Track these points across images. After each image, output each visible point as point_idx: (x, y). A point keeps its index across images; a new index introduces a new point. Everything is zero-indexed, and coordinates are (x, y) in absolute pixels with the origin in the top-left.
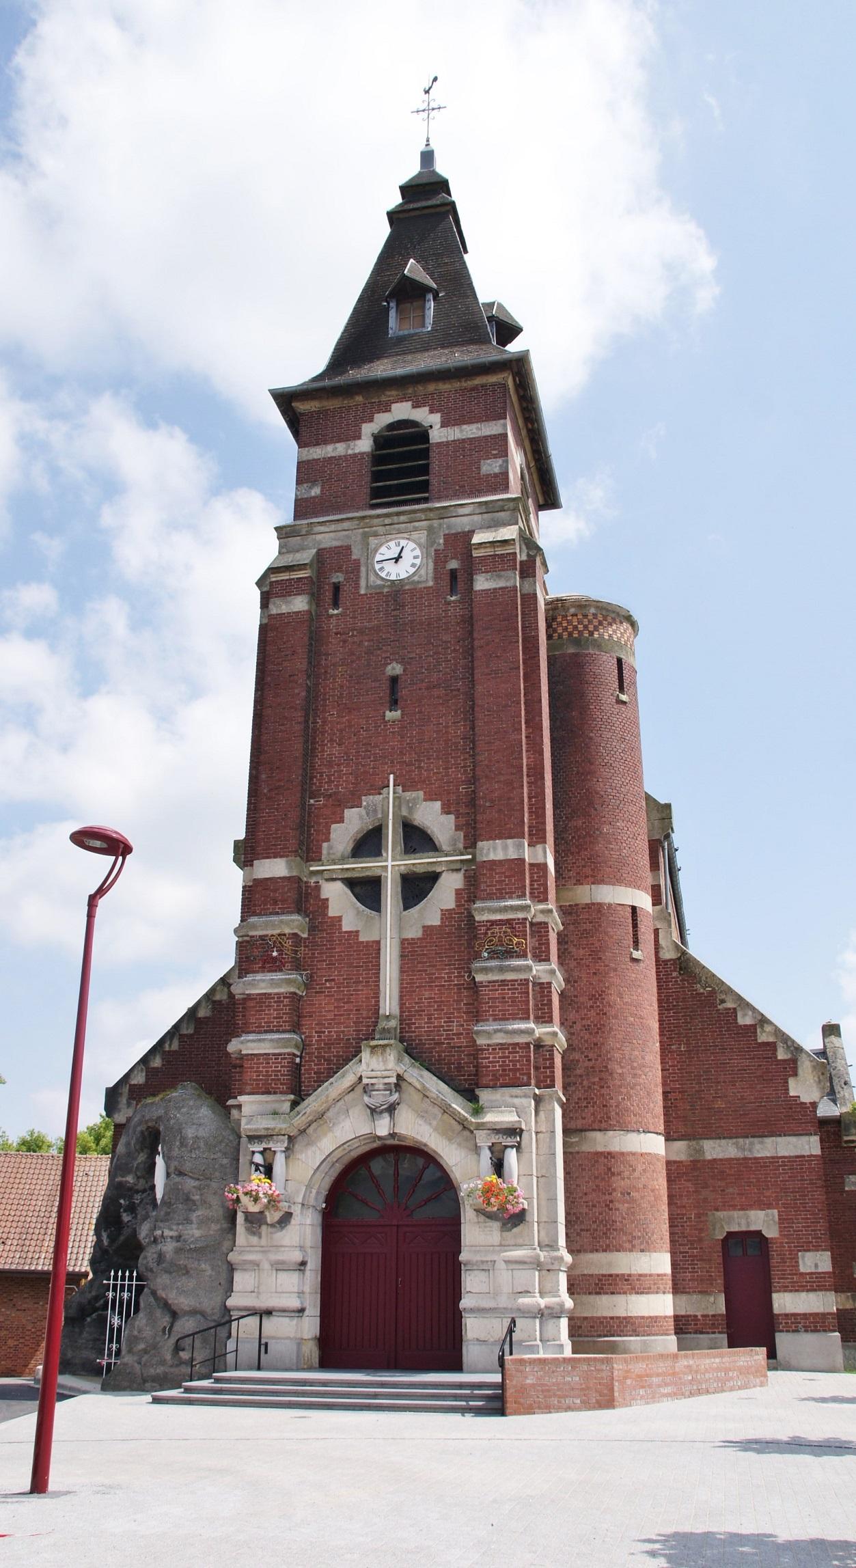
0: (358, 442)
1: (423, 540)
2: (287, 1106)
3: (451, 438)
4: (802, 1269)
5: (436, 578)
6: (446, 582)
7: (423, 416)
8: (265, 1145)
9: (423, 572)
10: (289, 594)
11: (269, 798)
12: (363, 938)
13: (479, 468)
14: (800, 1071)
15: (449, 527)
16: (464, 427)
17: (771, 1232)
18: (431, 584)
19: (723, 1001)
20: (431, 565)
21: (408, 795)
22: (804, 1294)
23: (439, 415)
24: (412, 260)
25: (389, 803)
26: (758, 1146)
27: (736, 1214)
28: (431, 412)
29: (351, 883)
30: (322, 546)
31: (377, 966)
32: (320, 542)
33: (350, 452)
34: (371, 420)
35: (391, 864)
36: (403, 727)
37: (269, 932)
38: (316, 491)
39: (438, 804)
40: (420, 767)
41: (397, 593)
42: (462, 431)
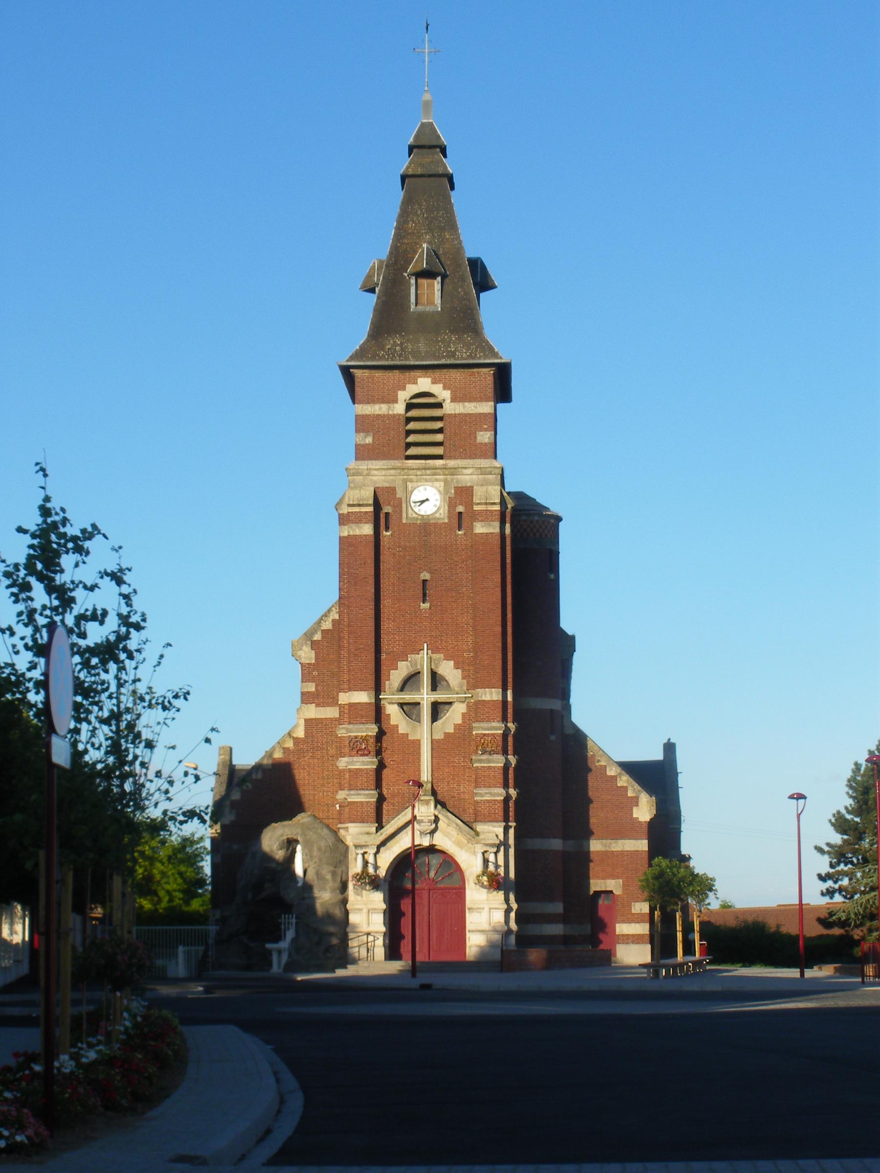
0: (396, 405)
1: (442, 489)
2: (374, 830)
3: (457, 412)
4: (633, 911)
5: (449, 517)
6: (455, 521)
7: (442, 393)
8: (364, 850)
9: (441, 511)
10: (360, 522)
11: (355, 655)
12: (410, 738)
13: (475, 438)
14: (640, 804)
15: (457, 482)
16: (466, 404)
17: (618, 892)
18: (446, 521)
19: (599, 761)
20: (447, 508)
21: (435, 656)
22: (633, 925)
23: (449, 392)
24: (439, 309)
25: (423, 660)
26: (614, 845)
27: (599, 881)
28: (445, 388)
29: (401, 705)
30: (377, 485)
31: (419, 754)
32: (375, 482)
33: (391, 412)
34: (404, 389)
35: (425, 697)
36: (431, 614)
37: (360, 734)
38: (369, 440)
39: (452, 663)
40: (442, 640)
41: (426, 526)
42: (464, 407)
